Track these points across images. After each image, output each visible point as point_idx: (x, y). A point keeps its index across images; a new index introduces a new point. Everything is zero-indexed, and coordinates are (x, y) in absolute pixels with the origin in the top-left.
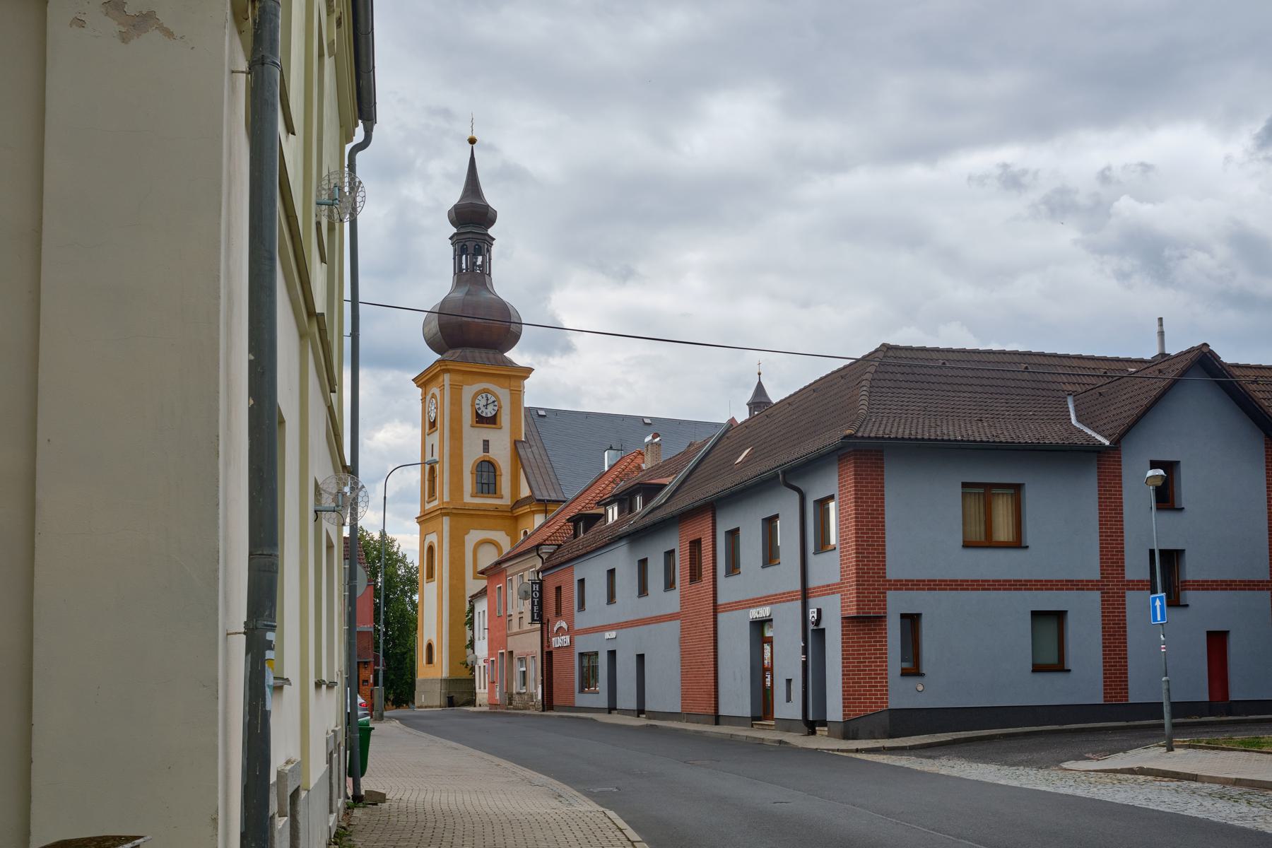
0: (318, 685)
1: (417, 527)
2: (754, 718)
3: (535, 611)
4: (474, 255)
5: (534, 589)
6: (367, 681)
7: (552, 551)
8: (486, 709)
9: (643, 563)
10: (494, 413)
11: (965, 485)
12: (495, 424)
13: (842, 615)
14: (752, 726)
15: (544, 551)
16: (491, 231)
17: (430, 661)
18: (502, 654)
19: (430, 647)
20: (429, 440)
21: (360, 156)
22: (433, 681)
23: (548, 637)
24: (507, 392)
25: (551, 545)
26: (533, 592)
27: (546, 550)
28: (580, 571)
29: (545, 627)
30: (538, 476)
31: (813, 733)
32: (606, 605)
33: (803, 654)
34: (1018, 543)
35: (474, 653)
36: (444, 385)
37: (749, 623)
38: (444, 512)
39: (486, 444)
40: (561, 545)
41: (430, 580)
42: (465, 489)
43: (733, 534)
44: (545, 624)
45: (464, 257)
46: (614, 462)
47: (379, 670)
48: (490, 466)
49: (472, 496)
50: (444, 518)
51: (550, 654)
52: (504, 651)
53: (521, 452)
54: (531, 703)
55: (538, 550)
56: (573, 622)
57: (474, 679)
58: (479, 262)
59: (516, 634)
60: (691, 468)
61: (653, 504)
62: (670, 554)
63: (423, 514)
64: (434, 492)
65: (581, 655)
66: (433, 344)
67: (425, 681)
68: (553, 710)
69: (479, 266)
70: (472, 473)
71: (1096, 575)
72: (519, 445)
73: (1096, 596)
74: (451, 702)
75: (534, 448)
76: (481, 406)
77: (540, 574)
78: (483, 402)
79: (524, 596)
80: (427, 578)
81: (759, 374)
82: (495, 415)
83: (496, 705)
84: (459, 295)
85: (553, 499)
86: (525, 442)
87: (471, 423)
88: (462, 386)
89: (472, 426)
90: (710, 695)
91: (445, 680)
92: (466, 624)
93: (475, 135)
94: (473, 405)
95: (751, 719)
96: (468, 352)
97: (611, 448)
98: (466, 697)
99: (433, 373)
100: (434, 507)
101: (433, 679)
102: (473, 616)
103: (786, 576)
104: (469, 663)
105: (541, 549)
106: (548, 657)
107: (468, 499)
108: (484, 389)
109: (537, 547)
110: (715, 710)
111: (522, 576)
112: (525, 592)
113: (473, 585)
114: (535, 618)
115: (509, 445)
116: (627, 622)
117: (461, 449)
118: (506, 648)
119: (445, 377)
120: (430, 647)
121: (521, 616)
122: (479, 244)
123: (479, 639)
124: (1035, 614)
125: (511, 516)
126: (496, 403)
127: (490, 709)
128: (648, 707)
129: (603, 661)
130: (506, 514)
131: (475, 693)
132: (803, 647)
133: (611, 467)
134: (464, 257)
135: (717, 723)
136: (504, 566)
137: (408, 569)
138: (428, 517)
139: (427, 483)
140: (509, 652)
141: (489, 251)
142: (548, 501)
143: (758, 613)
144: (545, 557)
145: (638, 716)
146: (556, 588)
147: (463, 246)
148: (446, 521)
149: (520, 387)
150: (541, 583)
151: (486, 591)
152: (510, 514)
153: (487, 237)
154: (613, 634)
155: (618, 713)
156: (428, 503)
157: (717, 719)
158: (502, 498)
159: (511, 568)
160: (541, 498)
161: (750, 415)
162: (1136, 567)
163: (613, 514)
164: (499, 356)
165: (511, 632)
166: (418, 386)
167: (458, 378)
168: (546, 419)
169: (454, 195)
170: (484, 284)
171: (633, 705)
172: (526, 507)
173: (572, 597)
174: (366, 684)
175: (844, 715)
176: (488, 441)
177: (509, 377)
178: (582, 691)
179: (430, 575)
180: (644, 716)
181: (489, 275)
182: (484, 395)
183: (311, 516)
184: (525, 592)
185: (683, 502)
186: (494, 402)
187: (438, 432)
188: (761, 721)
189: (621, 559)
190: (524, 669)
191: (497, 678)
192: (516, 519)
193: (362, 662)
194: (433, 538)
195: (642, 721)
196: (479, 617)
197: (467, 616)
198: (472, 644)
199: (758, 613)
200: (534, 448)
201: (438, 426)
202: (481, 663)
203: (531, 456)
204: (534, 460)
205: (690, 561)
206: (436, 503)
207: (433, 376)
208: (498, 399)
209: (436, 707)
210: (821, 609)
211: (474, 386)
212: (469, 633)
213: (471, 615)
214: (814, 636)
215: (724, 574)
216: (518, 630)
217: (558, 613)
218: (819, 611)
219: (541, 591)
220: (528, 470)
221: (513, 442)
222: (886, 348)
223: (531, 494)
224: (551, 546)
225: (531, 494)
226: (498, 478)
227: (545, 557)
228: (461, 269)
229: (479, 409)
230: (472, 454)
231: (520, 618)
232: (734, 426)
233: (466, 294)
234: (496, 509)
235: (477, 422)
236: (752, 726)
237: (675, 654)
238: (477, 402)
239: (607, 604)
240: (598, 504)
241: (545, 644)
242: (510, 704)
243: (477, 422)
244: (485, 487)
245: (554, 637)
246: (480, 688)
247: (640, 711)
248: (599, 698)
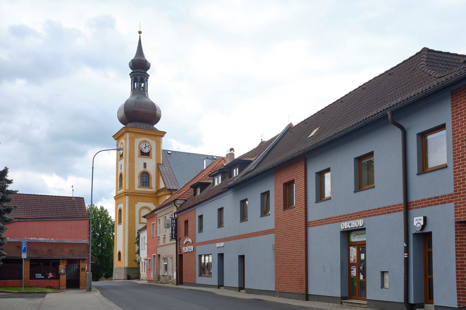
1: (114, 201)
2: (343, 298)
3: (173, 234)
4: (140, 82)
5: (173, 222)
6: (84, 269)
7: (182, 203)
8: (146, 282)
12: (149, 156)
13: (455, 219)
14: (342, 304)
15: (178, 203)
16: (148, 72)
17: (119, 259)
18: (154, 256)
19: (119, 253)
20: (120, 163)
22: (121, 268)
23: (180, 247)
25: (181, 200)
26: (172, 224)
27: (179, 202)
28: (199, 211)
29: (178, 242)
30: (168, 179)
32: (217, 228)
33: (405, 253)
35: (139, 256)
36: (126, 138)
37: (340, 232)
38: (126, 194)
39: (145, 164)
40: (187, 200)
41: (120, 224)
42: (136, 184)
44: (178, 240)
45: (136, 83)
46: (209, 165)
48: (147, 174)
49: (138, 187)
50: (126, 196)
52: (155, 254)
53: (161, 168)
54: (170, 281)
55: (175, 202)
56: (195, 238)
57: (140, 268)
58: (142, 86)
60: (268, 150)
62: (266, 195)
63: (117, 195)
64: (122, 186)
66: (122, 121)
67: (117, 268)
68: (182, 284)
69: (143, 88)
70: (139, 177)
72: (160, 166)
74: (129, 278)
75: (166, 167)
76: (143, 148)
77: (176, 215)
78: (144, 146)
79: (167, 226)
80: (119, 223)
82: (149, 152)
83: (151, 280)
84: (134, 99)
85: (175, 189)
86: (162, 164)
87: (138, 155)
88: (135, 139)
90: (301, 281)
91: (126, 268)
92: (136, 243)
93: (141, 30)
94: (139, 147)
95: (340, 299)
96: (137, 124)
98: (135, 276)
99: (121, 133)
100: (121, 192)
101: (121, 268)
102: (139, 239)
104: (138, 261)
105: (177, 202)
106: (180, 257)
108: (144, 140)
110: (306, 291)
111: (165, 217)
112: (168, 224)
113: (139, 227)
114: (173, 237)
115: (155, 165)
116: (232, 237)
117: (134, 166)
118: (156, 253)
119: (127, 134)
120: (119, 253)
121: (164, 237)
122: (143, 77)
123: (142, 250)
125: (156, 196)
126: (149, 147)
127: (148, 282)
128: (248, 285)
130: (153, 195)
131: (140, 274)
132: (405, 247)
133: (207, 167)
134: (136, 83)
135: (307, 299)
136: (156, 213)
137: (112, 222)
139: (118, 181)
140: (158, 255)
141: (147, 81)
142: (172, 189)
143: (219, 245)
144: (178, 206)
145: (239, 291)
146: (185, 221)
147: (135, 78)
148: (127, 198)
149: (160, 140)
150: (176, 219)
151: (147, 227)
152: (155, 196)
153: (146, 75)
154: (222, 244)
155: (225, 289)
156: (119, 190)
157: (307, 297)
158: (152, 188)
159: (159, 214)
160: (169, 188)
161: (221, 182)
164: (151, 126)
165: (159, 245)
166: (115, 139)
167: (133, 135)
168: (171, 155)
169: (132, 55)
170: (145, 95)
171: (236, 285)
172: (162, 192)
173: (195, 226)
174: (84, 270)
175: (458, 302)
176: (146, 163)
177: (155, 136)
178: (200, 275)
179: (120, 222)
180: (244, 291)
181: (147, 91)
182: (144, 143)
184: (168, 224)
186: (148, 146)
187: (124, 159)
188: (347, 299)
190: (166, 263)
191: (152, 268)
192: (158, 198)
193: (81, 259)
195: (242, 295)
196: (142, 240)
197: (136, 240)
198: (138, 252)
199: (219, 245)
200: (166, 167)
201: (124, 156)
202: (143, 260)
203: (165, 170)
204: (166, 172)
205: (284, 196)
206: (122, 190)
207: (121, 134)
208: (150, 145)
209: (122, 280)
210: (426, 217)
211: (140, 139)
212: (137, 247)
213: (138, 239)
215: (315, 201)
216: (163, 244)
217: (186, 234)
219: (176, 223)
220: (164, 176)
221: (157, 164)
222: (425, 50)
223: (165, 187)
224: (181, 201)
225: (165, 187)
226: (150, 180)
227: (178, 206)
228: (134, 88)
229: (142, 149)
230: (139, 169)
231: (164, 238)
232: (292, 127)
233: (137, 98)
236: (342, 304)
237: (270, 255)
238: (141, 146)
239: (218, 228)
241: (178, 251)
242: (159, 280)
244: (145, 183)
245: (183, 247)
246: (142, 272)
247: (241, 288)
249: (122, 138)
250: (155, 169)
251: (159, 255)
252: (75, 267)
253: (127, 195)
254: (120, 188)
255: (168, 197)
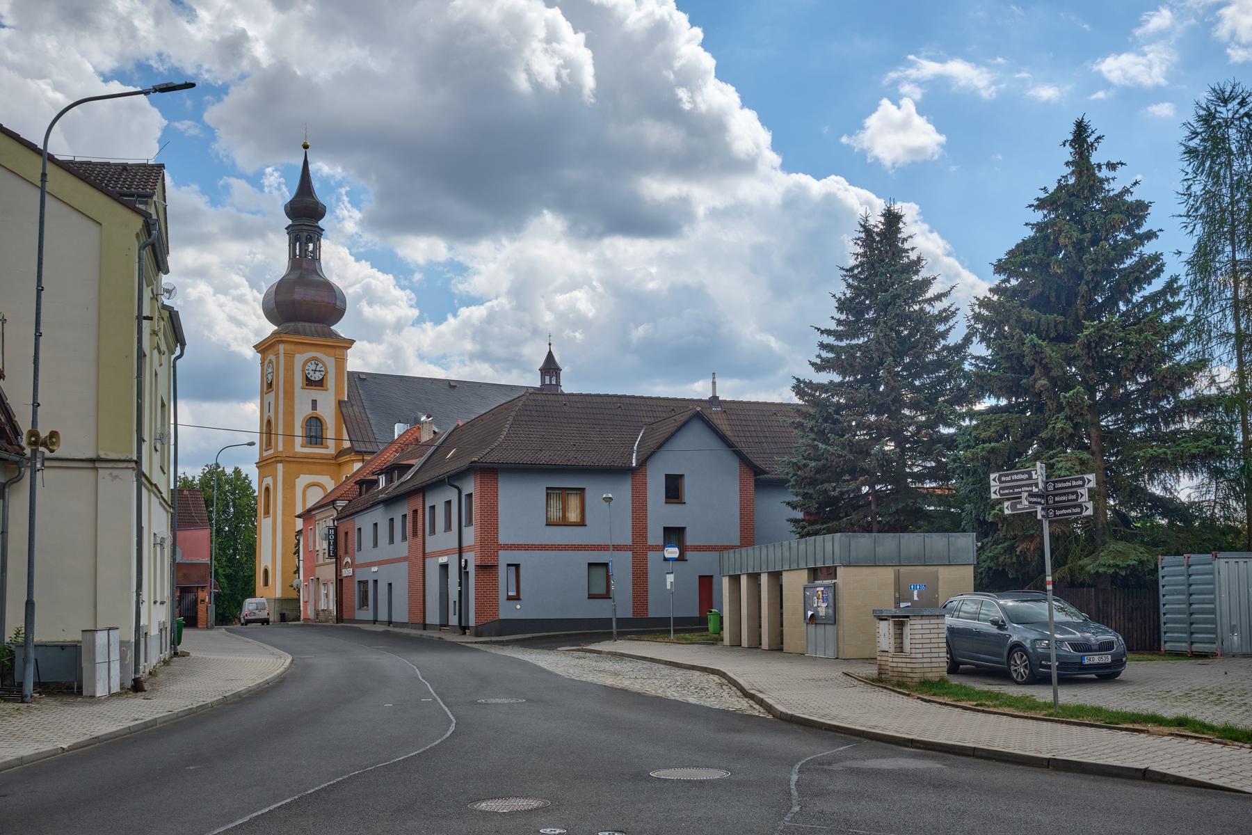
0: (155, 603)
1: (257, 470)
9: (392, 520)
10: (321, 377)
11: (547, 488)
12: (322, 386)
17: (266, 584)
19: (266, 571)
21: (178, 362)
24: (333, 360)
31: (465, 633)
34: (582, 523)
39: (314, 403)
43: (433, 508)
47: (215, 588)
51: (341, 580)
59: (321, 565)
61: (403, 480)
62: (405, 516)
65: (359, 582)
66: (270, 315)
69: (311, 252)
71: (629, 542)
73: (629, 554)
77: (336, 522)
78: (313, 367)
81: (550, 344)
89: (303, 388)
97: (400, 422)
103: (451, 540)
104: (295, 586)
106: (340, 582)
107: (298, 449)
109: (333, 502)
115: (333, 404)
117: (293, 407)
120: (266, 571)
124: (590, 565)
126: (323, 373)
129: (371, 585)
135: (425, 629)
138: (264, 463)
147: (296, 236)
149: (344, 355)
153: (318, 230)
156: (266, 451)
159: (319, 515)
160: (359, 449)
162: (655, 535)
163: (382, 481)
167: (292, 347)
176: (316, 401)
177: (335, 347)
178: (360, 608)
183: (152, 546)
185: (425, 478)
189: (378, 516)
194: (268, 481)
206: (271, 452)
214: (463, 573)
217: (346, 553)
218: (466, 561)
219: (336, 534)
220: (349, 426)
226: (324, 431)
229: (309, 373)
230: (302, 411)
234: (323, 457)
235: (307, 385)
238: (307, 368)
240: (373, 474)
242: (317, 618)
243: (307, 385)
247: (390, 623)
248: (367, 614)
249: (271, 351)
250: (334, 410)
251: (318, 579)
252: (191, 596)
253: (280, 462)
254: (266, 447)
255: (357, 466)
